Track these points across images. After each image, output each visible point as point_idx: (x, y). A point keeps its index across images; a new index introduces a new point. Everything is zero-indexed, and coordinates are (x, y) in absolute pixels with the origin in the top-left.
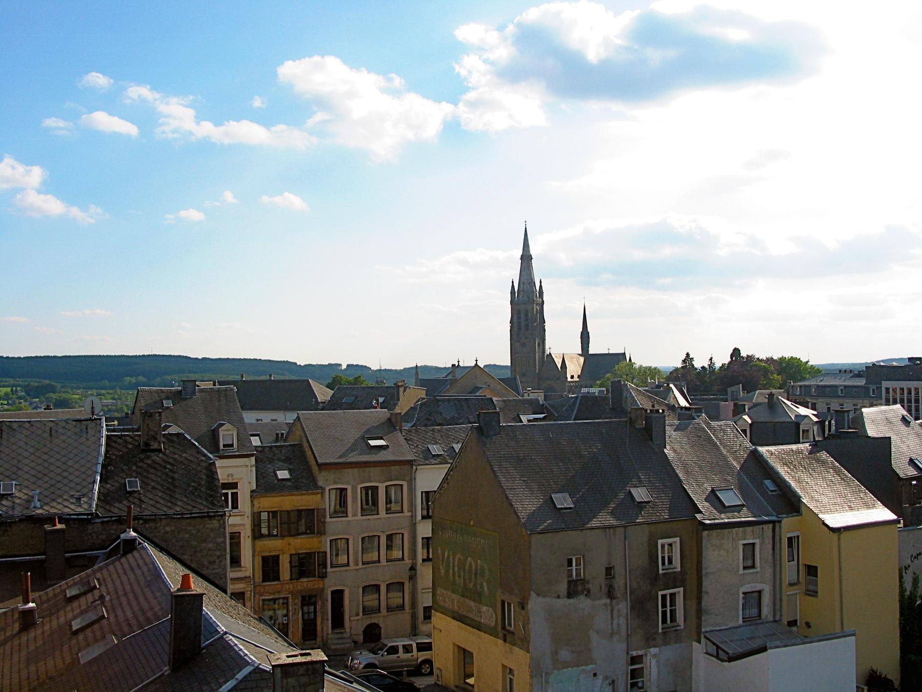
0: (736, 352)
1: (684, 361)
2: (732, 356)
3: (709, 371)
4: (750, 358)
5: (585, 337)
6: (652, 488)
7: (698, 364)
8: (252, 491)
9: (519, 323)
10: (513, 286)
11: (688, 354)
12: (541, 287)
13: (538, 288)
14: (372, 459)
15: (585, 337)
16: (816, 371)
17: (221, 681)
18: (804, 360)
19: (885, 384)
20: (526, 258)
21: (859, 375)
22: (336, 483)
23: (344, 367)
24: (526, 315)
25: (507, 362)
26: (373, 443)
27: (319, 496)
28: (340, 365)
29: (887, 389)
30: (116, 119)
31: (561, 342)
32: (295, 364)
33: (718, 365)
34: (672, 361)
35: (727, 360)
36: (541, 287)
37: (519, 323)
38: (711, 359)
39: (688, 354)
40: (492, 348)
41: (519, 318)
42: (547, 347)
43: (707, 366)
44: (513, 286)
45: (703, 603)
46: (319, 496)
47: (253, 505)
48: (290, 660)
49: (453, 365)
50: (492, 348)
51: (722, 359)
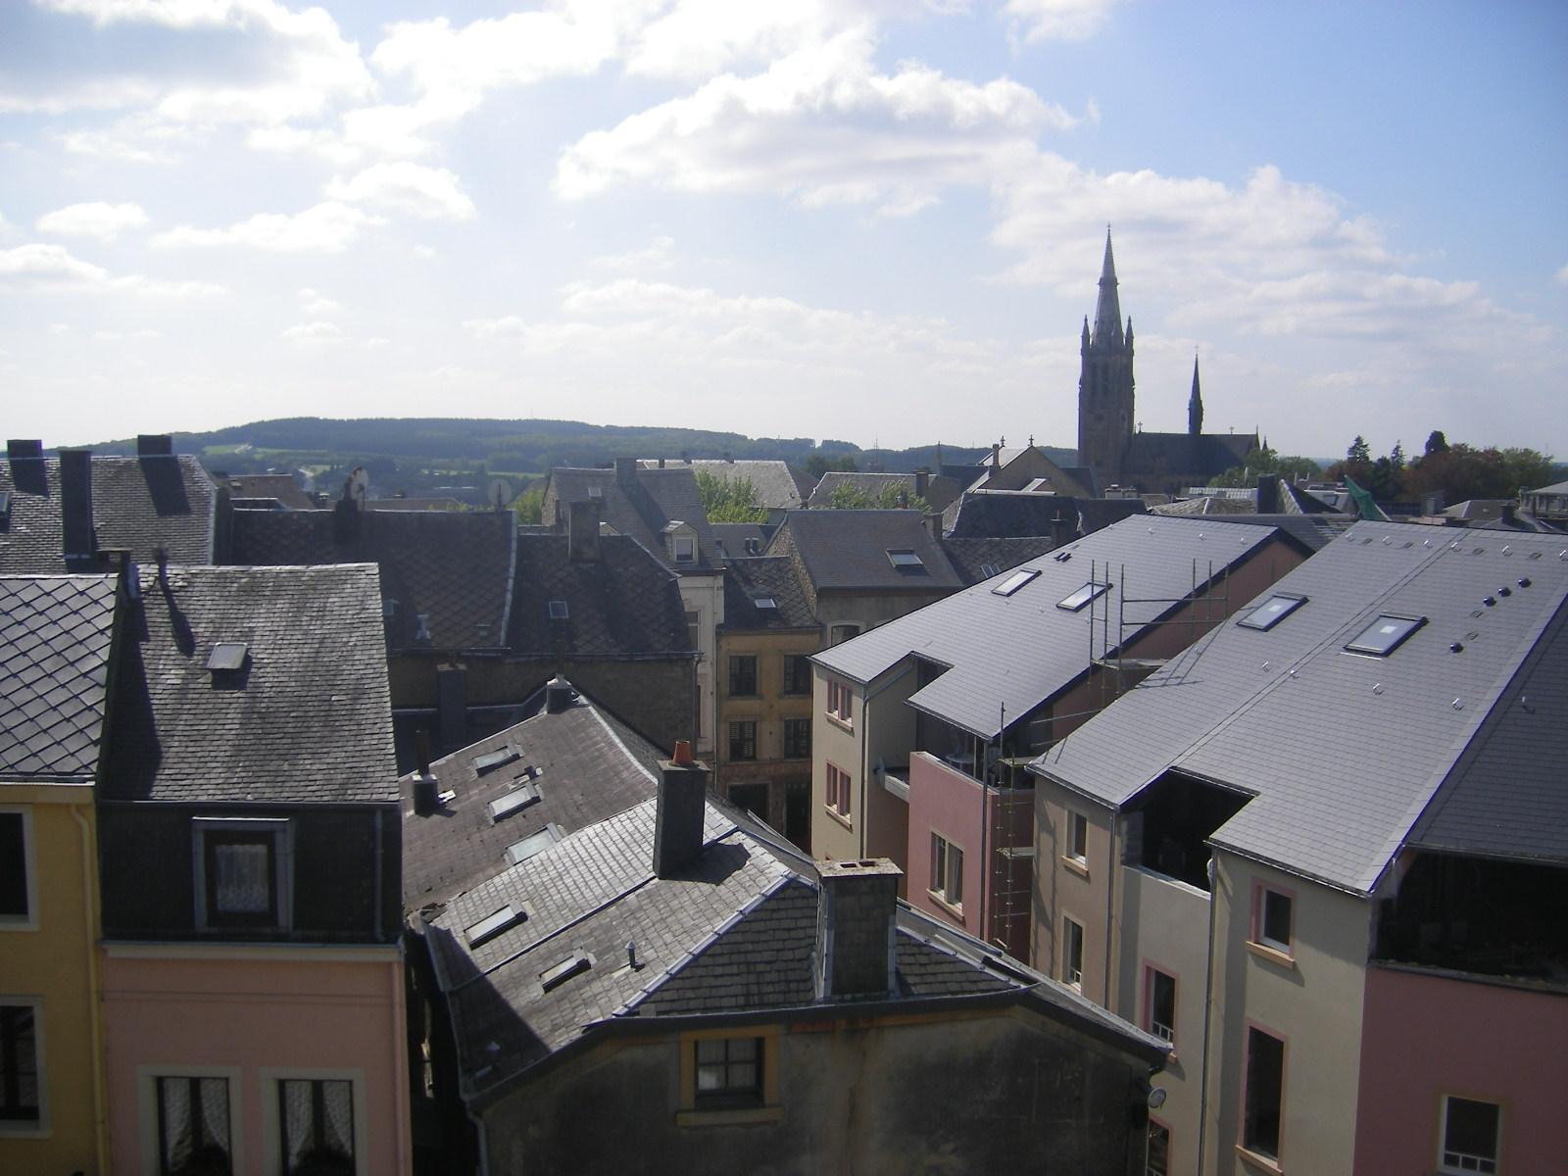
0: (1436, 440)
1: (1352, 450)
2: (1429, 445)
3: (1388, 468)
4: (1460, 449)
6: (436, 776)
7: (1374, 456)
8: (719, 626)
10: (1086, 328)
11: (1359, 440)
14: (918, 584)
18: (1543, 455)
22: (842, 617)
23: (818, 444)
25: (1074, 445)
27: (818, 636)
28: (811, 441)
30: (632, 121)
32: (745, 438)
33: (1408, 458)
34: (1336, 451)
35: (1421, 452)
38: (1397, 448)
39: (1359, 440)
40: (1182, 427)
42: (1136, 422)
43: (1389, 457)
44: (1086, 328)
46: (818, 636)
47: (719, 648)
48: (849, 872)
50: (1182, 427)
51: (1414, 449)
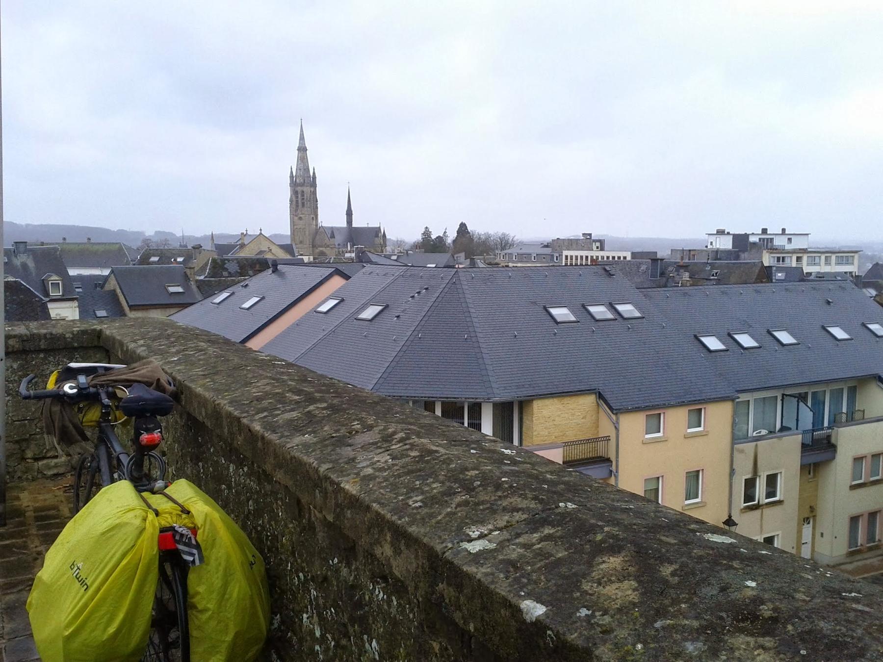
5: (349, 213)
9: (297, 201)
10: (292, 172)
12: (314, 173)
13: (311, 174)
15: (349, 213)
16: (522, 244)
17: (116, 476)
19: (565, 253)
20: (302, 149)
21: (547, 246)
24: (303, 195)
26: (247, 305)
29: (567, 257)
31: (330, 216)
36: (314, 173)
37: (297, 201)
41: (297, 197)
44: (292, 172)
45: (366, 380)
49: (242, 234)
